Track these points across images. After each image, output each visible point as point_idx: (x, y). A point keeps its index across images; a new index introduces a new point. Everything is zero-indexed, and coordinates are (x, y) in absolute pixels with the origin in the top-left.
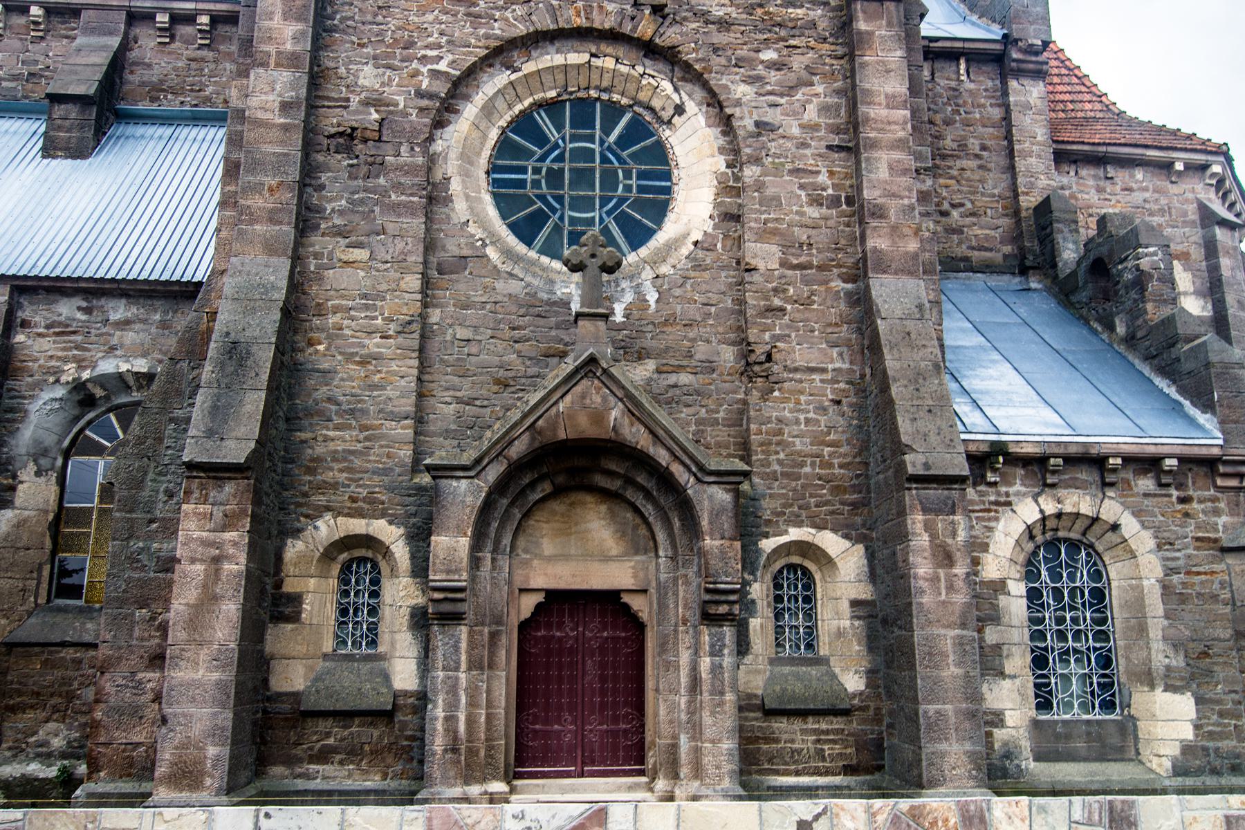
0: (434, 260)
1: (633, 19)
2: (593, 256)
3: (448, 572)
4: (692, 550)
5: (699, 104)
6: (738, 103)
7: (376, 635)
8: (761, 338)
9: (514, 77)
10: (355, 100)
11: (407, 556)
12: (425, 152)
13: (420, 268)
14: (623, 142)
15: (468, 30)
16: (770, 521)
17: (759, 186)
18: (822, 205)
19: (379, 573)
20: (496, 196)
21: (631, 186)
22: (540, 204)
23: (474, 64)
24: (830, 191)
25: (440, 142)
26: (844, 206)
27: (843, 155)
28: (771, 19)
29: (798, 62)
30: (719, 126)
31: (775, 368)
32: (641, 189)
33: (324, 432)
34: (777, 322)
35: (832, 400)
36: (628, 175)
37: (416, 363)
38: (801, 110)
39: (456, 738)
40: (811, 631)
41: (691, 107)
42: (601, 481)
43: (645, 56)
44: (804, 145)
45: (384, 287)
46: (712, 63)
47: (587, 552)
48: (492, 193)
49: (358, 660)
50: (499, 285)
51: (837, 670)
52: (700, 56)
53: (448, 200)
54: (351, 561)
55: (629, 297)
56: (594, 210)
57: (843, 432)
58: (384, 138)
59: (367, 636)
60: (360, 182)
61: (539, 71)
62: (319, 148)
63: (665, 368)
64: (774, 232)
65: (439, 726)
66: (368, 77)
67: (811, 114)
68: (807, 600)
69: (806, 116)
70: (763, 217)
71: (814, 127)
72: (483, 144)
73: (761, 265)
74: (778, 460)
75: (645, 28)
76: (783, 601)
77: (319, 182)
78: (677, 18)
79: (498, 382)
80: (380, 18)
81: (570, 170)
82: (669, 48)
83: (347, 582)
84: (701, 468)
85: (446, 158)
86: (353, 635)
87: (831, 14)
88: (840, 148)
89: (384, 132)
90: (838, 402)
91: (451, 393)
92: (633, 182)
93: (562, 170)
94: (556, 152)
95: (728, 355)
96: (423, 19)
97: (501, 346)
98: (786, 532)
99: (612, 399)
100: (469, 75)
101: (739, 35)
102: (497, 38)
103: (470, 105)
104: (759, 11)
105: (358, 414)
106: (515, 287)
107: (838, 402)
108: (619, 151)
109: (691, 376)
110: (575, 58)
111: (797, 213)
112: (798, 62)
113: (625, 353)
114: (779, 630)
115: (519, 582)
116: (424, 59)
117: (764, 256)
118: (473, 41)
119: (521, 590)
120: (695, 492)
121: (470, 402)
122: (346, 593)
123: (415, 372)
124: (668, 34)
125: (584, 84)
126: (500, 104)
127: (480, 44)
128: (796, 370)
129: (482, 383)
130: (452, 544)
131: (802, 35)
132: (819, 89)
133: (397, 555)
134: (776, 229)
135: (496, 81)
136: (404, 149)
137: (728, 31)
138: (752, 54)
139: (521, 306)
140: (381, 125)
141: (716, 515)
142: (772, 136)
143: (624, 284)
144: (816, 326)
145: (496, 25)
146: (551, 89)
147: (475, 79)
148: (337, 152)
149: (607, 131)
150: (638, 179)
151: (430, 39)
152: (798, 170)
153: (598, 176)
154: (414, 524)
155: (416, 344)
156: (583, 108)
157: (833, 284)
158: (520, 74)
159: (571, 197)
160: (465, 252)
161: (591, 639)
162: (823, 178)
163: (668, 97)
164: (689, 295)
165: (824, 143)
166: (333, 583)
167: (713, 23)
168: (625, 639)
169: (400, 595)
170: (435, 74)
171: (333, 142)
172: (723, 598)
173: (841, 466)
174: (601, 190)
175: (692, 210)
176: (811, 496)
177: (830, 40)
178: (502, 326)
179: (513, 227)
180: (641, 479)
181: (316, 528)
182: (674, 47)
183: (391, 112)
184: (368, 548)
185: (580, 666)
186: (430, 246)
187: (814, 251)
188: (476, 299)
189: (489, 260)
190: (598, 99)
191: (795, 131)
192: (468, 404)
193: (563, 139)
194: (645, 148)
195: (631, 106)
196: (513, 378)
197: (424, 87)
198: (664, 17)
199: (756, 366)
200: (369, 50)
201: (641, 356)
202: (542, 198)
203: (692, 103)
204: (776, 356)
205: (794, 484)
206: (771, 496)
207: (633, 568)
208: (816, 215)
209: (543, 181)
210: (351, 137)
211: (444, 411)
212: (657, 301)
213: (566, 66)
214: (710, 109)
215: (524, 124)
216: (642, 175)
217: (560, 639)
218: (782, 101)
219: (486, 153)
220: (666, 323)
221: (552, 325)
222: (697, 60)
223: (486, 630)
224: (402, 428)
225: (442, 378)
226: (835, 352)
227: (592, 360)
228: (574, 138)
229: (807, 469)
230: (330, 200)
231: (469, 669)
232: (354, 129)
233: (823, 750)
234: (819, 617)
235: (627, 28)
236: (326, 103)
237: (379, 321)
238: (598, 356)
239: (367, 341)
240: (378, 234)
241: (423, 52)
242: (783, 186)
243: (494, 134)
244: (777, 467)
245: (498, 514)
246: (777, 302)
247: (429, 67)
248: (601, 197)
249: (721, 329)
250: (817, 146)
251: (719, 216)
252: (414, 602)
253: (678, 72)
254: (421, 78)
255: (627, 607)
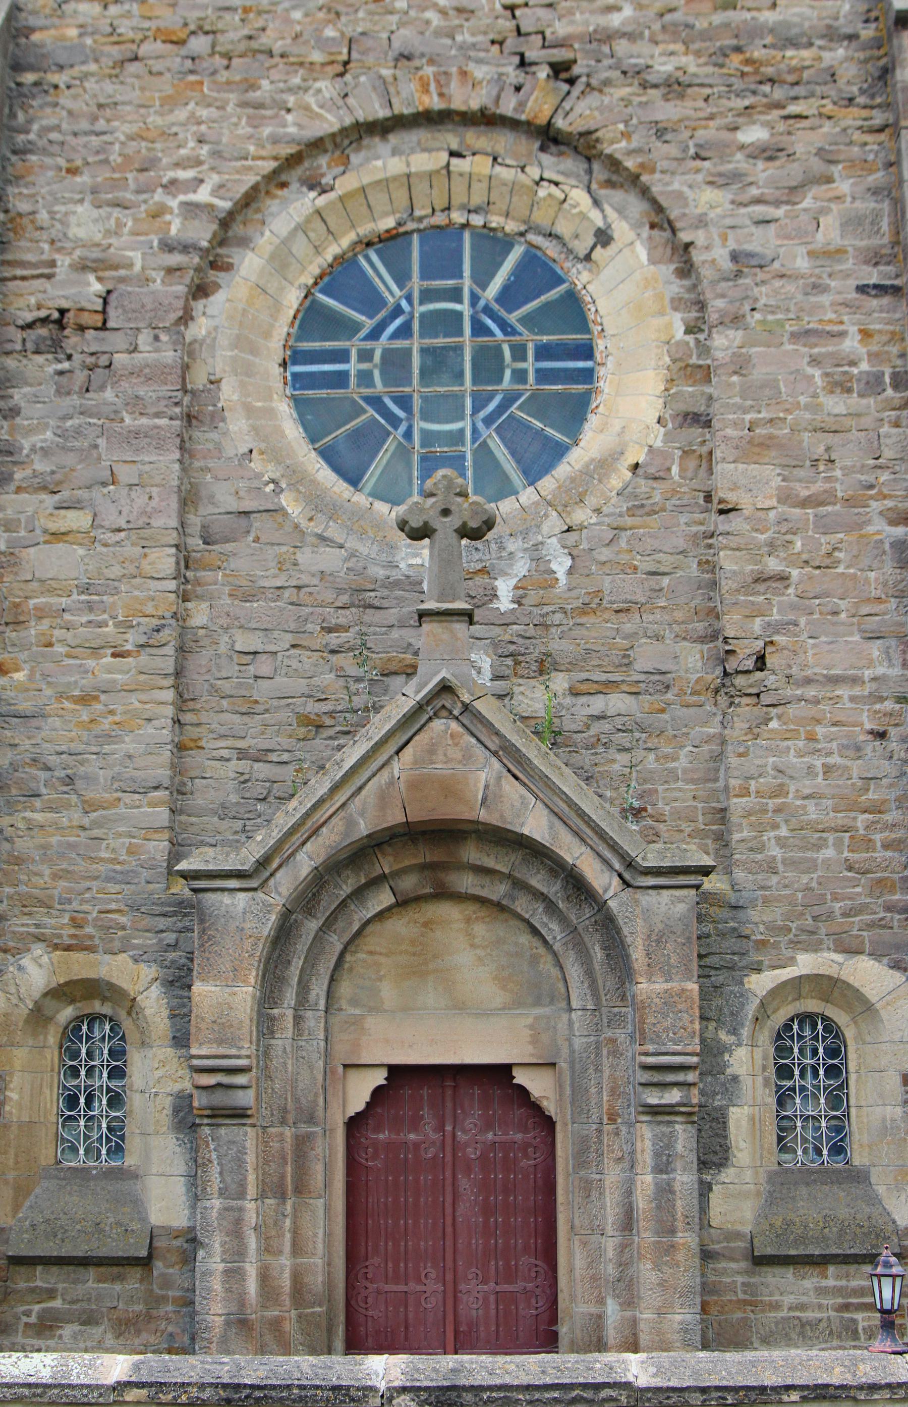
0: (195, 521)
1: (518, 89)
2: (446, 512)
3: (220, 1042)
4: (623, 997)
5: (636, 226)
6: (702, 222)
7: (122, 1137)
8: (744, 629)
9: (322, 201)
10: (63, 261)
11: (165, 1013)
12: (179, 341)
13: (173, 538)
14: (510, 296)
15: (244, 129)
16: (763, 943)
17: (741, 365)
18: (849, 391)
19: (123, 1038)
20: (298, 403)
21: (525, 372)
22: (371, 412)
23: (255, 188)
24: (864, 366)
25: (203, 320)
26: (890, 392)
27: (886, 300)
28: (757, 72)
29: (804, 142)
30: (671, 261)
31: (771, 680)
32: (543, 376)
33: (28, 814)
34: (776, 599)
35: (871, 732)
36: (519, 353)
37: (169, 695)
38: (812, 227)
39: (242, 1303)
40: (839, 1128)
41: (622, 230)
42: (467, 883)
43: (543, 149)
44: (818, 288)
45: (116, 571)
46: (654, 155)
47: (455, 1000)
48: (293, 398)
49: (95, 1178)
50: (304, 557)
51: (881, 1190)
52: (634, 144)
53: (218, 416)
54: (79, 1019)
55: (521, 567)
56: (462, 418)
57: (891, 785)
58: (110, 324)
59: (108, 1140)
60: (75, 400)
61: (363, 189)
62: (9, 347)
63: (584, 687)
64: (765, 444)
65: (217, 1285)
66: (85, 223)
67: (830, 232)
68: (833, 1071)
69: (820, 236)
70: (748, 417)
71: (834, 254)
72: (274, 317)
73: (744, 500)
74: (778, 839)
75: (539, 103)
76: (791, 1076)
77: (11, 403)
78: (594, 82)
79: (305, 720)
80: (101, 125)
81: (424, 351)
82: (581, 135)
83: (75, 1055)
84: (630, 864)
85: (212, 347)
86: (87, 1138)
87: (861, 55)
88: (881, 289)
89: (112, 312)
90: (882, 735)
91: (230, 742)
92: (530, 365)
93: (408, 352)
94: (398, 322)
95: (693, 662)
96: (171, 118)
97: (308, 660)
98: (792, 961)
99: (479, 751)
100: (247, 205)
101: (701, 104)
102: (292, 141)
103: (250, 255)
104: (735, 60)
105: (79, 784)
106: (329, 559)
107: (882, 735)
108: (503, 313)
109: (629, 699)
110: (425, 161)
111: (807, 407)
112: (804, 142)
113: (517, 663)
114: (784, 1126)
115: (342, 1053)
116: (172, 186)
117: (753, 484)
118: (252, 148)
119: (346, 1066)
120: (621, 904)
121: (261, 756)
122: (74, 1072)
123: (170, 711)
124: (578, 110)
125: (440, 204)
126: (300, 246)
127: (263, 153)
128: (808, 681)
129: (280, 724)
130: (226, 996)
131: (812, 95)
132: (844, 186)
133: (148, 1012)
134: (771, 437)
135: (294, 208)
136: (144, 339)
137: (682, 96)
138: (726, 135)
139: (340, 591)
140: (105, 302)
141: (656, 940)
142: (761, 276)
143: (512, 545)
144: (843, 604)
145: (289, 118)
146: (386, 214)
147: (258, 210)
148: (37, 352)
149: (482, 280)
150: (538, 357)
151: (183, 152)
152: (808, 332)
153: (468, 357)
154: (173, 962)
155: (169, 666)
156: (442, 238)
157: (870, 529)
158: (332, 195)
159: (425, 399)
160: (248, 505)
161: (466, 1144)
162: (851, 344)
163: (583, 216)
164: (624, 558)
165: (853, 283)
166: (52, 1055)
167: (655, 86)
168: (525, 1146)
169: (155, 1076)
170: (191, 209)
171: (32, 335)
172: (671, 1078)
173: (886, 846)
174: (475, 381)
175: (630, 407)
176: (835, 899)
177: (861, 100)
178: (309, 627)
179: (328, 455)
180: (538, 880)
181: (20, 968)
182: (589, 133)
183: (122, 280)
184: (104, 999)
185: (449, 1189)
186: (188, 499)
187: (838, 473)
188: (266, 584)
189: (285, 514)
190: (466, 226)
191: (802, 263)
192: (257, 760)
193: (409, 298)
194: (547, 305)
195: (522, 234)
196: (331, 714)
197: (174, 230)
198: (571, 81)
199: (740, 675)
200: (84, 179)
201: (545, 666)
202: (375, 402)
203: (625, 225)
204: (771, 661)
205: (805, 879)
206: (766, 901)
207: (531, 1027)
208: (841, 409)
209: (377, 374)
210: (60, 324)
211: (218, 778)
212: (570, 572)
213: (408, 176)
214: (656, 233)
215: (341, 276)
216: (543, 352)
217: (417, 1145)
218: (780, 212)
219: (282, 328)
220: (585, 609)
221: (392, 620)
222: (630, 153)
223: (288, 1132)
224: (150, 805)
225: (214, 720)
226: (875, 649)
227: (445, 688)
228: (427, 295)
229: (829, 853)
230: (30, 431)
231: (262, 1196)
232: (62, 312)
233: (854, 1321)
234: (852, 1102)
235: (508, 107)
236: (19, 272)
237: (110, 629)
238: (454, 682)
239: (91, 663)
240: (104, 484)
241: (171, 174)
242: (784, 365)
243: (293, 299)
244: (776, 852)
245: (302, 945)
246: (773, 565)
247: (182, 198)
248: (474, 394)
249: (679, 615)
250: (843, 288)
251: (674, 417)
252: (177, 1087)
253: (600, 172)
254: (168, 217)
255: (523, 1091)
